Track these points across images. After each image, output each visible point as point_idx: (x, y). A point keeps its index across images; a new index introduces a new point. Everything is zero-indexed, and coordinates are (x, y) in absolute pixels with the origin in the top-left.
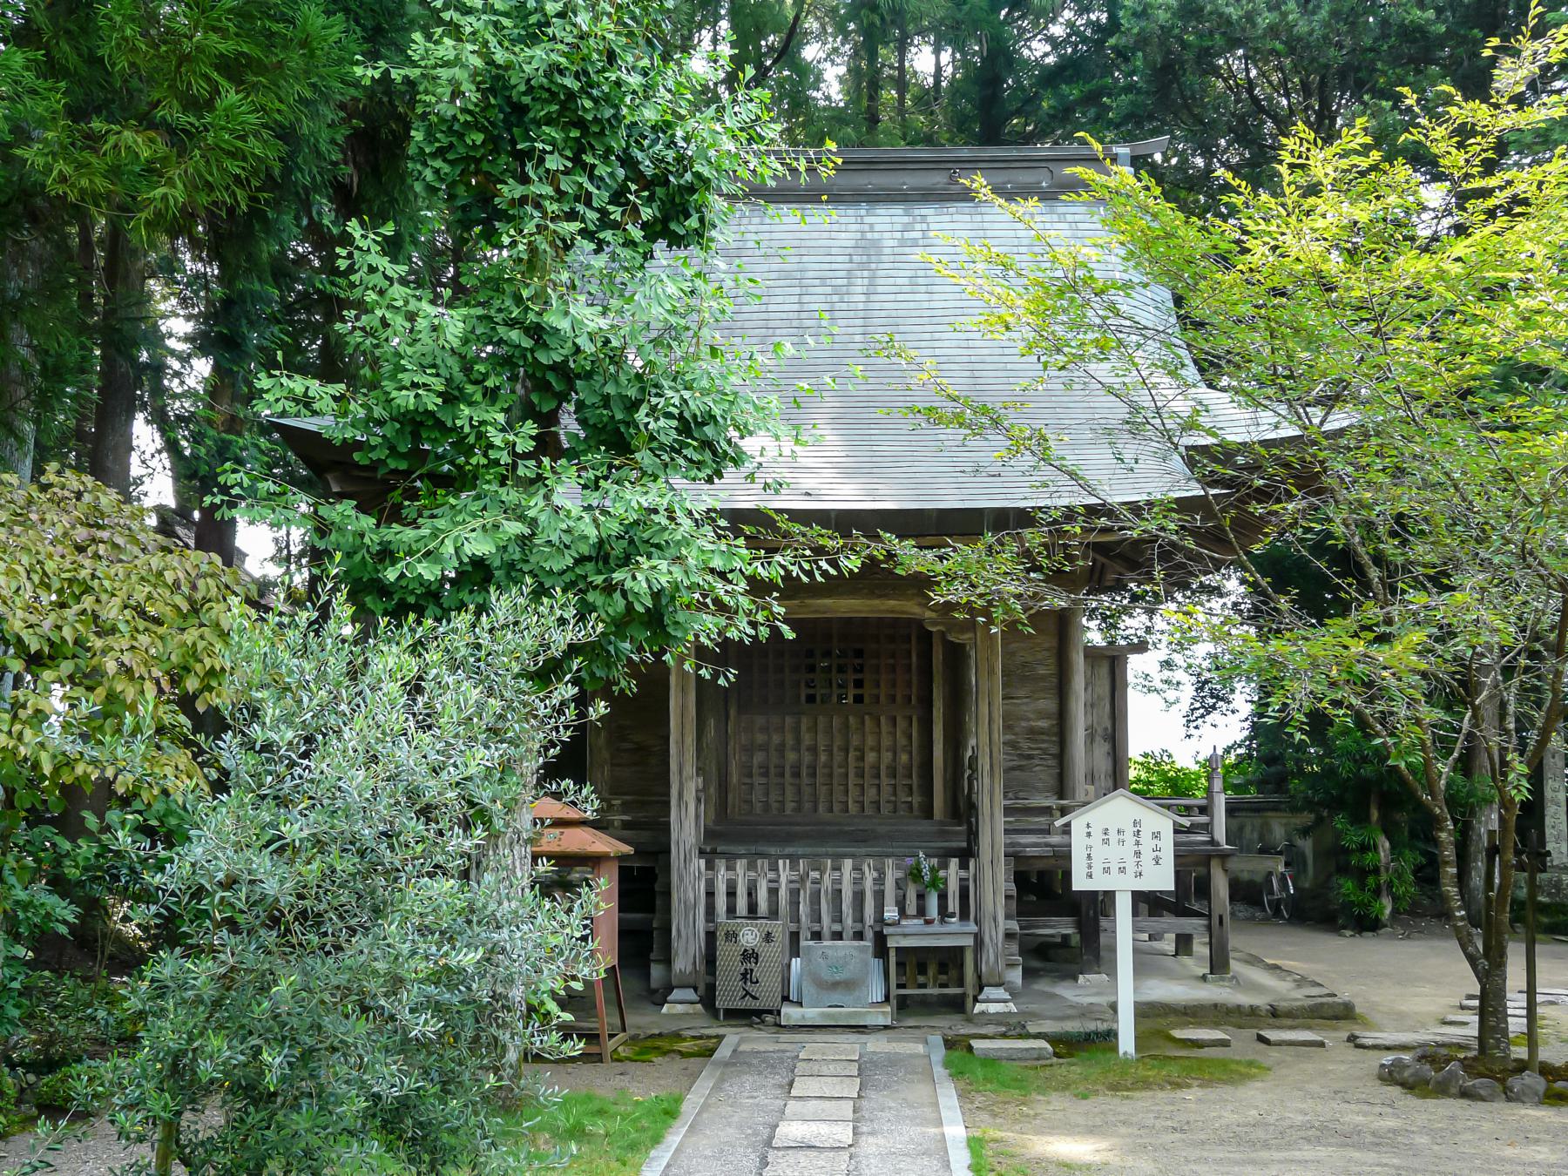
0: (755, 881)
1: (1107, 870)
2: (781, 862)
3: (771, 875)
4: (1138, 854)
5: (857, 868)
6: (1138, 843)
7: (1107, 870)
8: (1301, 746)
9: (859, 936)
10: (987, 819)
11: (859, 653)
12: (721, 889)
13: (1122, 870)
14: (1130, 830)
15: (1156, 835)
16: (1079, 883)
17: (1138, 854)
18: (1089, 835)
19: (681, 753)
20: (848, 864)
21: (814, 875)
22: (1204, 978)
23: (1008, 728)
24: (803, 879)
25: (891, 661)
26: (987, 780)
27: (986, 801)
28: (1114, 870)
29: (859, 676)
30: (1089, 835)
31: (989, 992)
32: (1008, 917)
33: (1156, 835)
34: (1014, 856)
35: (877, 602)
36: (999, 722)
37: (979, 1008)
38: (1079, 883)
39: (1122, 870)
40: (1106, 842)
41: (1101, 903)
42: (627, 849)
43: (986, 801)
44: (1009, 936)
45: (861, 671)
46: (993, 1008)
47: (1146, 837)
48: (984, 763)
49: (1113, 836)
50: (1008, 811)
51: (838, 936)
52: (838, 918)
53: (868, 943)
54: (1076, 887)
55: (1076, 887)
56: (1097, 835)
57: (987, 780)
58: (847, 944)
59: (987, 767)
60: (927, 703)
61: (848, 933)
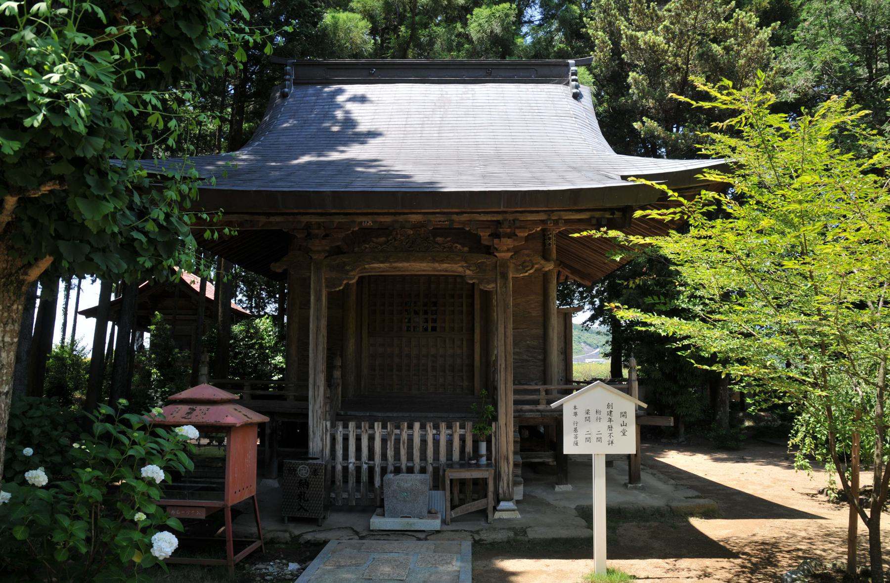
0: (360, 435)
1: (588, 440)
2: (376, 424)
3: (371, 432)
4: (610, 428)
5: (423, 427)
6: (610, 420)
7: (588, 440)
8: (80, 448)
9: (423, 470)
10: (503, 397)
11: (435, 304)
12: (340, 439)
13: (599, 440)
14: (605, 411)
15: (624, 414)
16: (569, 448)
17: (610, 428)
18: (576, 414)
19: (316, 356)
20: (417, 425)
21: (398, 431)
22: (625, 485)
23: (515, 344)
24: (389, 434)
25: (452, 308)
26: (503, 374)
27: (503, 386)
28: (594, 439)
29: (434, 317)
30: (576, 414)
31: (503, 505)
32: (515, 453)
33: (624, 414)
34: (519, 418)
35: (436, 265)
36: (510, 340)
37: (498, 515)
38: (569, 448)
39: (599, 440)
40: (588, 419)
41: (585, 462)
42: (265, 419)
43: (503, 386)
44: (516, 465)
45: (436, 314)
46: (505, 515)
47: (616, 415)
48: (501, 364)
49: (593, 415)
50: (516, 392)
51: (410, 470)
52: (410, 457)
53: (428, 477)
54: (566, 451)
55: (566, 451)
56: (582, 415)
57: (503, 374)
58: (417, 477)
59: (503, 366)
60: (472, 330)
61: (417, 468)
